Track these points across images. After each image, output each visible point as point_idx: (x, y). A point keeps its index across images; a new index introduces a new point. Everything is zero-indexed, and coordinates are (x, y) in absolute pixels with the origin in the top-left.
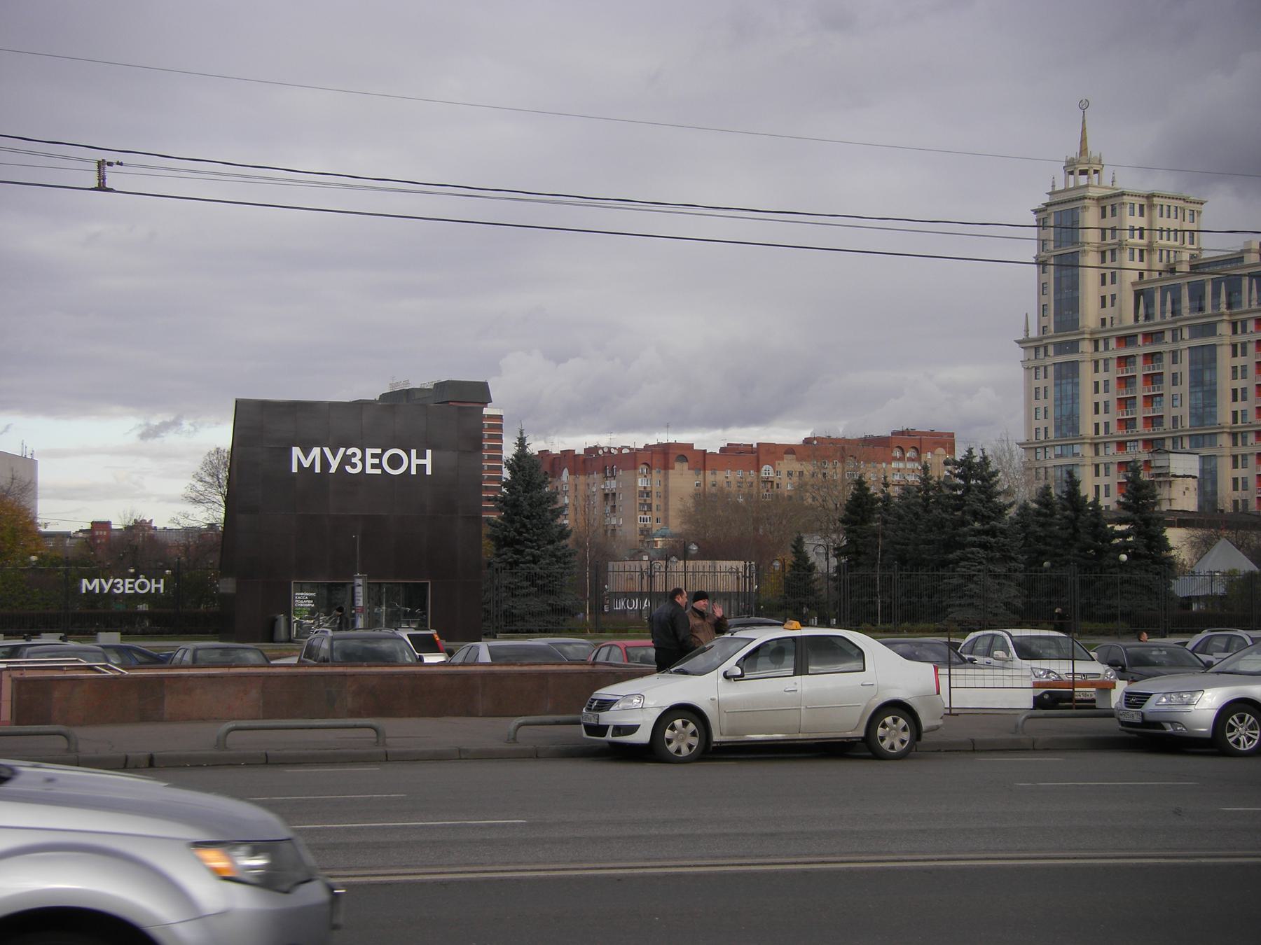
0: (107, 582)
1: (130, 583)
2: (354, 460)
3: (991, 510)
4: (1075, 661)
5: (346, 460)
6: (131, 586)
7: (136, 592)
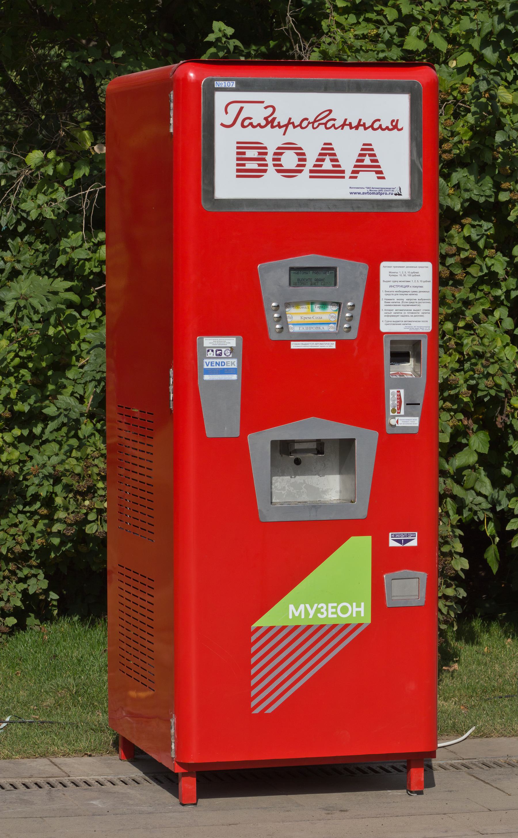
1: (332, 607)
6: (334, 610)
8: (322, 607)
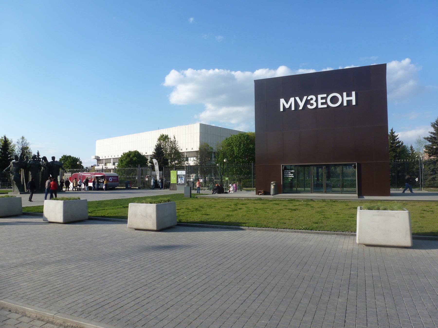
0: (301, 101)
1: (322, 98)
2: (311, 102)
5: (308, 102)
6: (324, 101)
7: (328, 106)
8: (312, 99)
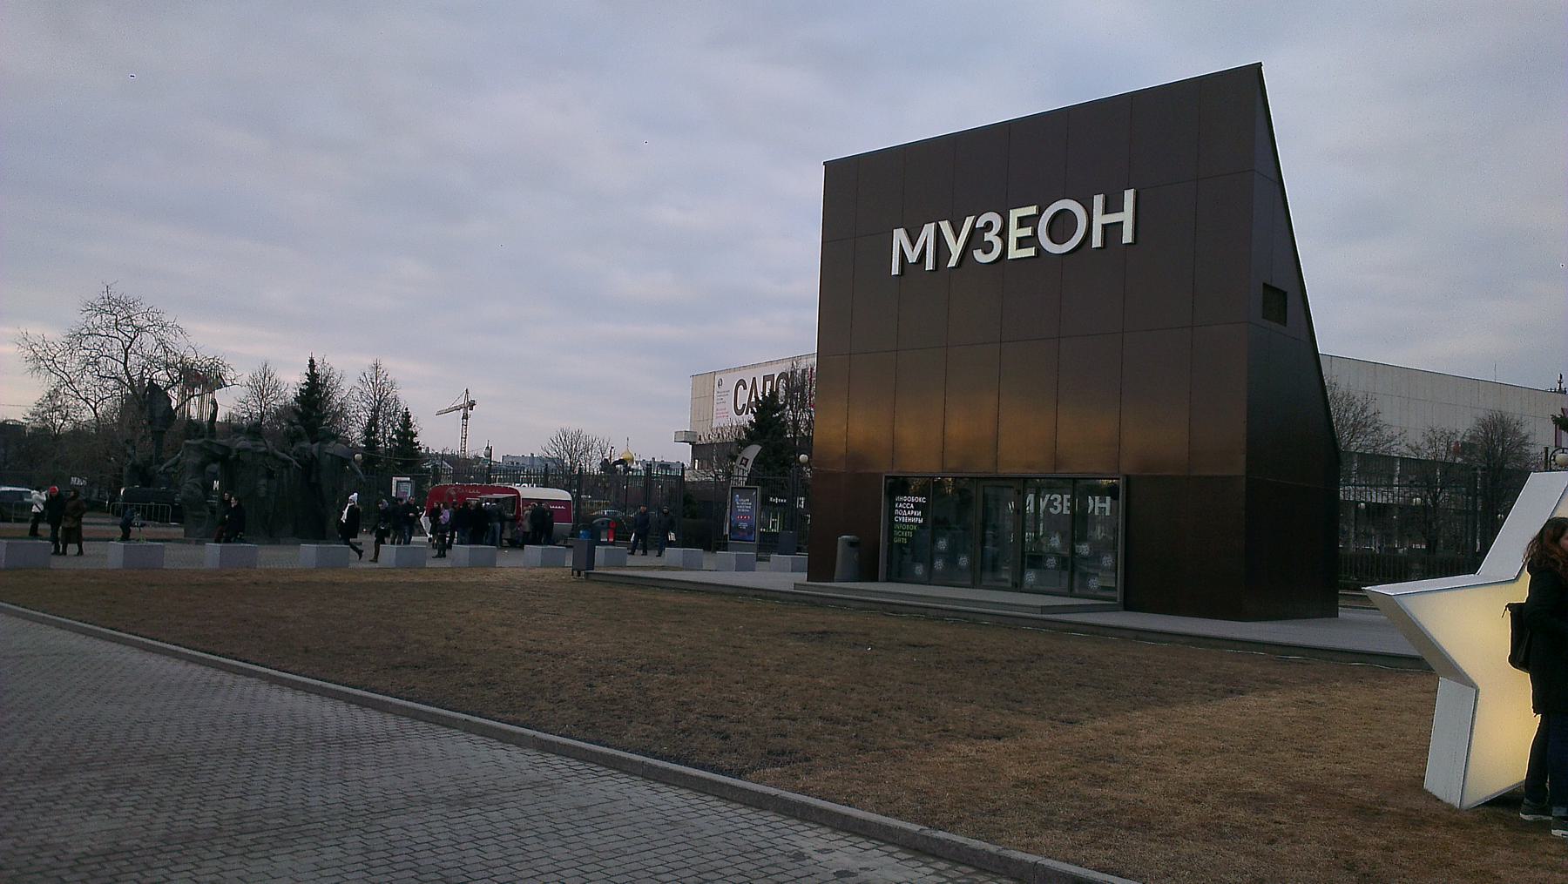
1: (1022, 222)
3: (948, 750)
4: (84, 543)
6: (1027, 232)
